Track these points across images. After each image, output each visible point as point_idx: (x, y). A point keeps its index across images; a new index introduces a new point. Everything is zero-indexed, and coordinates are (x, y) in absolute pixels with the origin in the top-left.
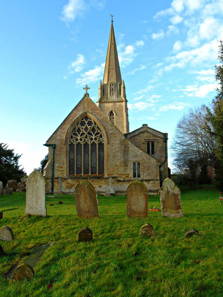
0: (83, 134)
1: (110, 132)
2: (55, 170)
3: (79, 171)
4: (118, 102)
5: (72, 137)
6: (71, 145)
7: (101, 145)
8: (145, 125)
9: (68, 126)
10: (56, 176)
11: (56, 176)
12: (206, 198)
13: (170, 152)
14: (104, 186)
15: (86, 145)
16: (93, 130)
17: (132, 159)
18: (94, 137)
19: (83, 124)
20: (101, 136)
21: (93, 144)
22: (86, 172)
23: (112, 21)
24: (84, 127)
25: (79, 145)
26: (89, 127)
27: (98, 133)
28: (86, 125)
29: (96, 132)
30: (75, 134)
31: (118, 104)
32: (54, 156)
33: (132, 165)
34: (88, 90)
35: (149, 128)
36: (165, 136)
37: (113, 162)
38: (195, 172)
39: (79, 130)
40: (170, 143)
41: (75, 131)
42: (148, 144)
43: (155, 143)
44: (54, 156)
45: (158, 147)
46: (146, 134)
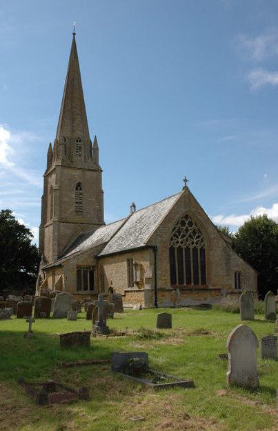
0: (183, 236)
1: (212, 236)
2: (157, 279)
4: (89, 170)
5: (172, 239)
6: (172, 249)
7: (203, 250)
9: (171, 226)
11: (158, 287)
12: (200, 310)
14: (209, 299)
15: (187, 249)
16: (194, 232)
21: (195, 249)
23: (74, 34)
24: (185, 228)
25: (180, 249)
26: (189, 228)
27: (198, 237)
28: (187, 225)
29: (181, 234)
31: (89, 173)
32: (155, 261)
33: (233, 275)
34: (187, 183)
36: (101, 223)
41: (177, 233)
44: (155, 261)
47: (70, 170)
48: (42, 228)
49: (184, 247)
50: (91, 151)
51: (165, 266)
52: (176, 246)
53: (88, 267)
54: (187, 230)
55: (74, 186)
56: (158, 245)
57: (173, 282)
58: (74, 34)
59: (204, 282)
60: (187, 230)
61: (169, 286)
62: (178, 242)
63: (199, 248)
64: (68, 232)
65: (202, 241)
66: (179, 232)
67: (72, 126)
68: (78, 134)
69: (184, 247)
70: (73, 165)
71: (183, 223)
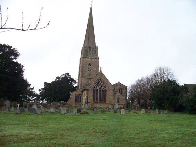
0: (99, 86)
3: (97, 100)
4: (94, 58)
5: (94, 87)
6: (94, 90)
7: (106, 90)
8: (119, 82)
10: (88, 101)
11: (88, 101)
13: (127, 93)
15: (100, 90)
16: (103, 85)
17: (117, 97)
18: (103, 88)
19: (99, 82)
20: (106, 87)
21: (100, 90)
22: (100, 100)
23: (91, 5)
25: (97, 90)
27: (104, 86)
30: (96, 86)
31: (93, 59)
35: (120, 83)
37: (110, 96)
38: (152, 110)
39: (97, 85)
40: (128, 91)
42: (120, 90)
43: (122, 90)
45: (124, 91)
46: (119, 86)
47: (86, 59)
48: (78, 79)
49: (99, 90)
50: (96, 50)
51: (91, 95)
52: (96, 89)
53: (79, 95)
54: (100, 84)
55: (88, 64)
56: (89, 89)
57: (94, 100)
58: (91, 5)
59: (105, 101)
60: (100, 84)
61: (92, 102)
62: (97, 88)
63: (104, 89)
64: (85, 82)
65: (106, 87)
66: (97, 85)
67: (88, 42)
68: (90, 45)
69: (99, 90)
70: (87, 57)
71: (99, 82)
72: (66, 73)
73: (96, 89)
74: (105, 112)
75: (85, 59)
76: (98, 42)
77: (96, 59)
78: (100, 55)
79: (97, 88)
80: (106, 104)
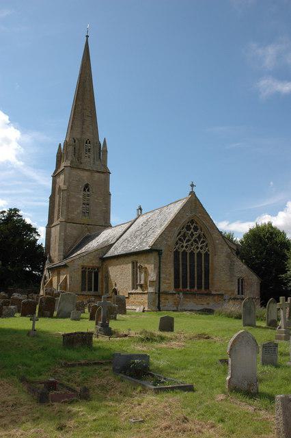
0: (188, 241)
5: (177, 243)
6: (176, 253)
7: (207, 255)
15: (192, 254)
16: (199, 237)
23: (87, 36)
27: (203, 242)
31: (97, 175)
48: (49, 228)
50: (101, 153)
51: (169, 270)
53: (93, 268)
54: (192, 235)
55: (81, 187)
56: (163, 248)
57: (177, 286)
58: (87, 36)
61: (172, 290)
63: (203, 252)
64: (75, 233)
65: (207, 246)
66: (184, 236)
68: (88, 135)
69: (189, 252)
70: (82, 166)
71: (188, 228)
72: (11, 210)
73: (181, 250)
74: (119, 316)
75: (74, 172)
76: (105, 132)
77: (102, 175)
78: (111, 164)
79: (182, 247)
80: (211, 297)
